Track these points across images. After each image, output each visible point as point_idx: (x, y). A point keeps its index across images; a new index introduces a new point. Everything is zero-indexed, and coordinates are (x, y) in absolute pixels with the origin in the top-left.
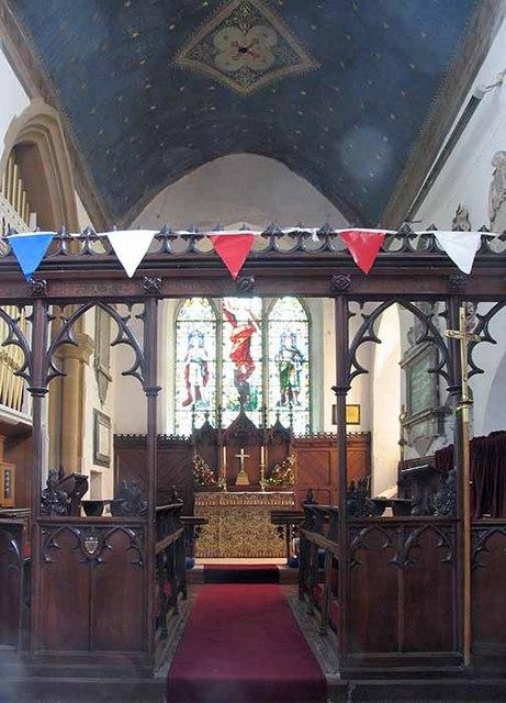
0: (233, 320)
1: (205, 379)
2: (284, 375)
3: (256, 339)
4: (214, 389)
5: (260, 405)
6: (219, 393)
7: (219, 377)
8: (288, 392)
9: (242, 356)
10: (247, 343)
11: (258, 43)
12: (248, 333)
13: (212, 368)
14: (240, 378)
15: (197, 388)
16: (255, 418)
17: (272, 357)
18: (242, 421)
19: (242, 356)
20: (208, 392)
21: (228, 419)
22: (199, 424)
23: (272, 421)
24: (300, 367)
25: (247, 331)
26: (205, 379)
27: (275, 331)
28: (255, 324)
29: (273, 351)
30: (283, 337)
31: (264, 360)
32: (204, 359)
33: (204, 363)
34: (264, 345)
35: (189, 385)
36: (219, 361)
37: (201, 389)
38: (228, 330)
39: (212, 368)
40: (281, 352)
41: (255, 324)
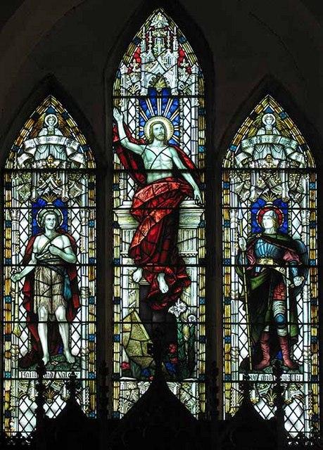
0: (136, 167)
1: (72, 310)
2: (257, 302)
3: (193, 217)
4: (54, 304)
5: (201, 366)
6: (104, 338)
7: (105, 300)
8: (270, 343)
9: (159, 253)
10: (172, 224)
11: (250, 13)
12: (174, 194)
13: (86, 282)
14: (153, 306)
15: (53, 325)
16: (190, 395)
17: (231, 254)
18: (158, 404)
19: (159, 253)
20: (77, 341)
21: (127, 393)
22: (55, 408)
23: (231, 402)
24: (297, 281)
25: (169, 193)
26: (72, 310)
27: (238, 197)
28: (189, 178)
29: (234, 240)
30: (257, 209)
31: (213, 263)
32: (69, 256)
33: (67, 270)
34: (213, 227)
35: (33, 320)
36: (104, 266)
37: (63, 331)
38: (125, 195)
39: (86, 282)
40: (252, 244)
41: (189, 178)
